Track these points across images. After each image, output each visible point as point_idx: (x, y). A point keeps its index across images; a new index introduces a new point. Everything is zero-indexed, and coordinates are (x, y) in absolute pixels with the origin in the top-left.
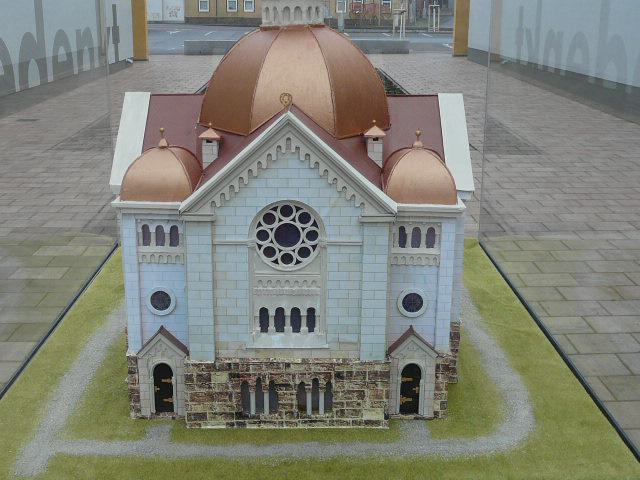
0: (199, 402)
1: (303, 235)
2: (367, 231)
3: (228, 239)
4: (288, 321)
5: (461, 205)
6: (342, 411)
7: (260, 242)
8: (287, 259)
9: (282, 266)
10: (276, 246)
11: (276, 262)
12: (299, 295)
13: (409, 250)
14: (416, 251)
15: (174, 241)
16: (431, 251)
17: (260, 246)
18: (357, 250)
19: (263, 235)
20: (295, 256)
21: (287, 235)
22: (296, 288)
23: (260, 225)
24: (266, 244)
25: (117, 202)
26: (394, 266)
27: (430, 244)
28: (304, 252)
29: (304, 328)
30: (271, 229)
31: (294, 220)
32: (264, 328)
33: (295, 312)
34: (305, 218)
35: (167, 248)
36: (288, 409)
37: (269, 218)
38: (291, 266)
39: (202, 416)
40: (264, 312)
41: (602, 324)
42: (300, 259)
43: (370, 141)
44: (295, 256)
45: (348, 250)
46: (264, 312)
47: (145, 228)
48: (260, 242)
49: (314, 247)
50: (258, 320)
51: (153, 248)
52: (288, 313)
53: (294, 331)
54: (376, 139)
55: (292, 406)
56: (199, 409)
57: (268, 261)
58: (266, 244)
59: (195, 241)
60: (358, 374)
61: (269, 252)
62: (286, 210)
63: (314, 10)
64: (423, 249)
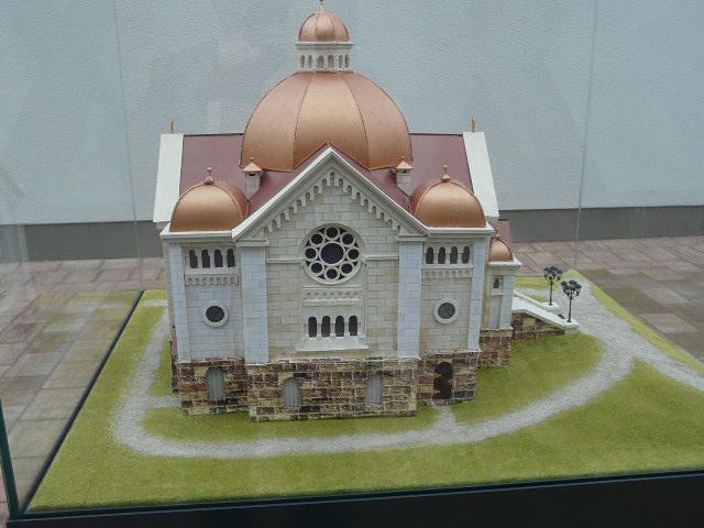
0: (267, 399)
1: (346, 253)
2: (402, 249)
3: (282, 259)
4: (347, 328)
5: (489, 228)
6: (391, 404)
7: (309, 260)
8: (332, 274)
9: (328, 281)
10: (322, 263)
11: (322, 277)
12: (317, 306)
13: (436, 265)
14: (454, 266)
15: (231, 263)
16: (465, 266)
17: (308, 263)
18: (392, 264)
19: (310, 253)
20: (339, 271)
21: (332, 253)
22: (317, 300)
23: (356, 245)
24: (313, 261)
25: (166, 232)
26: (428, 279)
27: (465, 260)
28: (347, 268)
29: (347, 333)
30: (318, 248)
31: (338, 240)
32: (313, 333)
33: (340, 320)
34: (348, 239)
35: (225, 270)
36: (345, 403)
37: (317, 239)
38: (335, 281)
39: (270, 410)
40: (312, 321)
41: (226, 380)
42: (343, 274)
43: (399, 175)
44: (339, 271)
45: (387, 264)
46: (312, 321)
47: (430, 251)
48: (309, 260)
49: (355, 264)
50: (307, 328)
51: (200, 271)
52: (347, 321)
53: (311, 336)
54: (405, 171)
55: (347, 400)
56: (267, 404)
57: (315, 276)
58: (313, 261)
59: (250, 268)
60: (406, 372)
61: (317, 268)
62: (332, 232)
63: (326, 59)
64: (460, 265)
